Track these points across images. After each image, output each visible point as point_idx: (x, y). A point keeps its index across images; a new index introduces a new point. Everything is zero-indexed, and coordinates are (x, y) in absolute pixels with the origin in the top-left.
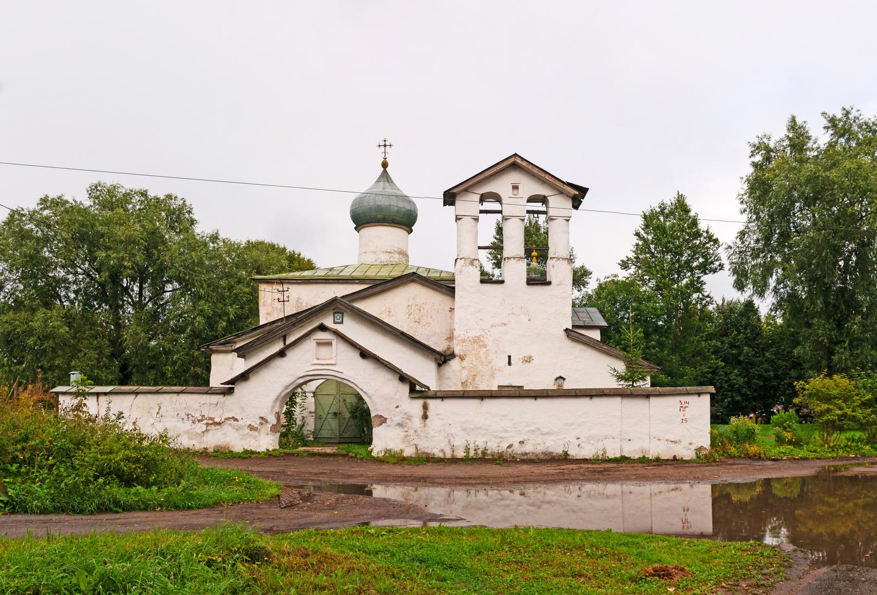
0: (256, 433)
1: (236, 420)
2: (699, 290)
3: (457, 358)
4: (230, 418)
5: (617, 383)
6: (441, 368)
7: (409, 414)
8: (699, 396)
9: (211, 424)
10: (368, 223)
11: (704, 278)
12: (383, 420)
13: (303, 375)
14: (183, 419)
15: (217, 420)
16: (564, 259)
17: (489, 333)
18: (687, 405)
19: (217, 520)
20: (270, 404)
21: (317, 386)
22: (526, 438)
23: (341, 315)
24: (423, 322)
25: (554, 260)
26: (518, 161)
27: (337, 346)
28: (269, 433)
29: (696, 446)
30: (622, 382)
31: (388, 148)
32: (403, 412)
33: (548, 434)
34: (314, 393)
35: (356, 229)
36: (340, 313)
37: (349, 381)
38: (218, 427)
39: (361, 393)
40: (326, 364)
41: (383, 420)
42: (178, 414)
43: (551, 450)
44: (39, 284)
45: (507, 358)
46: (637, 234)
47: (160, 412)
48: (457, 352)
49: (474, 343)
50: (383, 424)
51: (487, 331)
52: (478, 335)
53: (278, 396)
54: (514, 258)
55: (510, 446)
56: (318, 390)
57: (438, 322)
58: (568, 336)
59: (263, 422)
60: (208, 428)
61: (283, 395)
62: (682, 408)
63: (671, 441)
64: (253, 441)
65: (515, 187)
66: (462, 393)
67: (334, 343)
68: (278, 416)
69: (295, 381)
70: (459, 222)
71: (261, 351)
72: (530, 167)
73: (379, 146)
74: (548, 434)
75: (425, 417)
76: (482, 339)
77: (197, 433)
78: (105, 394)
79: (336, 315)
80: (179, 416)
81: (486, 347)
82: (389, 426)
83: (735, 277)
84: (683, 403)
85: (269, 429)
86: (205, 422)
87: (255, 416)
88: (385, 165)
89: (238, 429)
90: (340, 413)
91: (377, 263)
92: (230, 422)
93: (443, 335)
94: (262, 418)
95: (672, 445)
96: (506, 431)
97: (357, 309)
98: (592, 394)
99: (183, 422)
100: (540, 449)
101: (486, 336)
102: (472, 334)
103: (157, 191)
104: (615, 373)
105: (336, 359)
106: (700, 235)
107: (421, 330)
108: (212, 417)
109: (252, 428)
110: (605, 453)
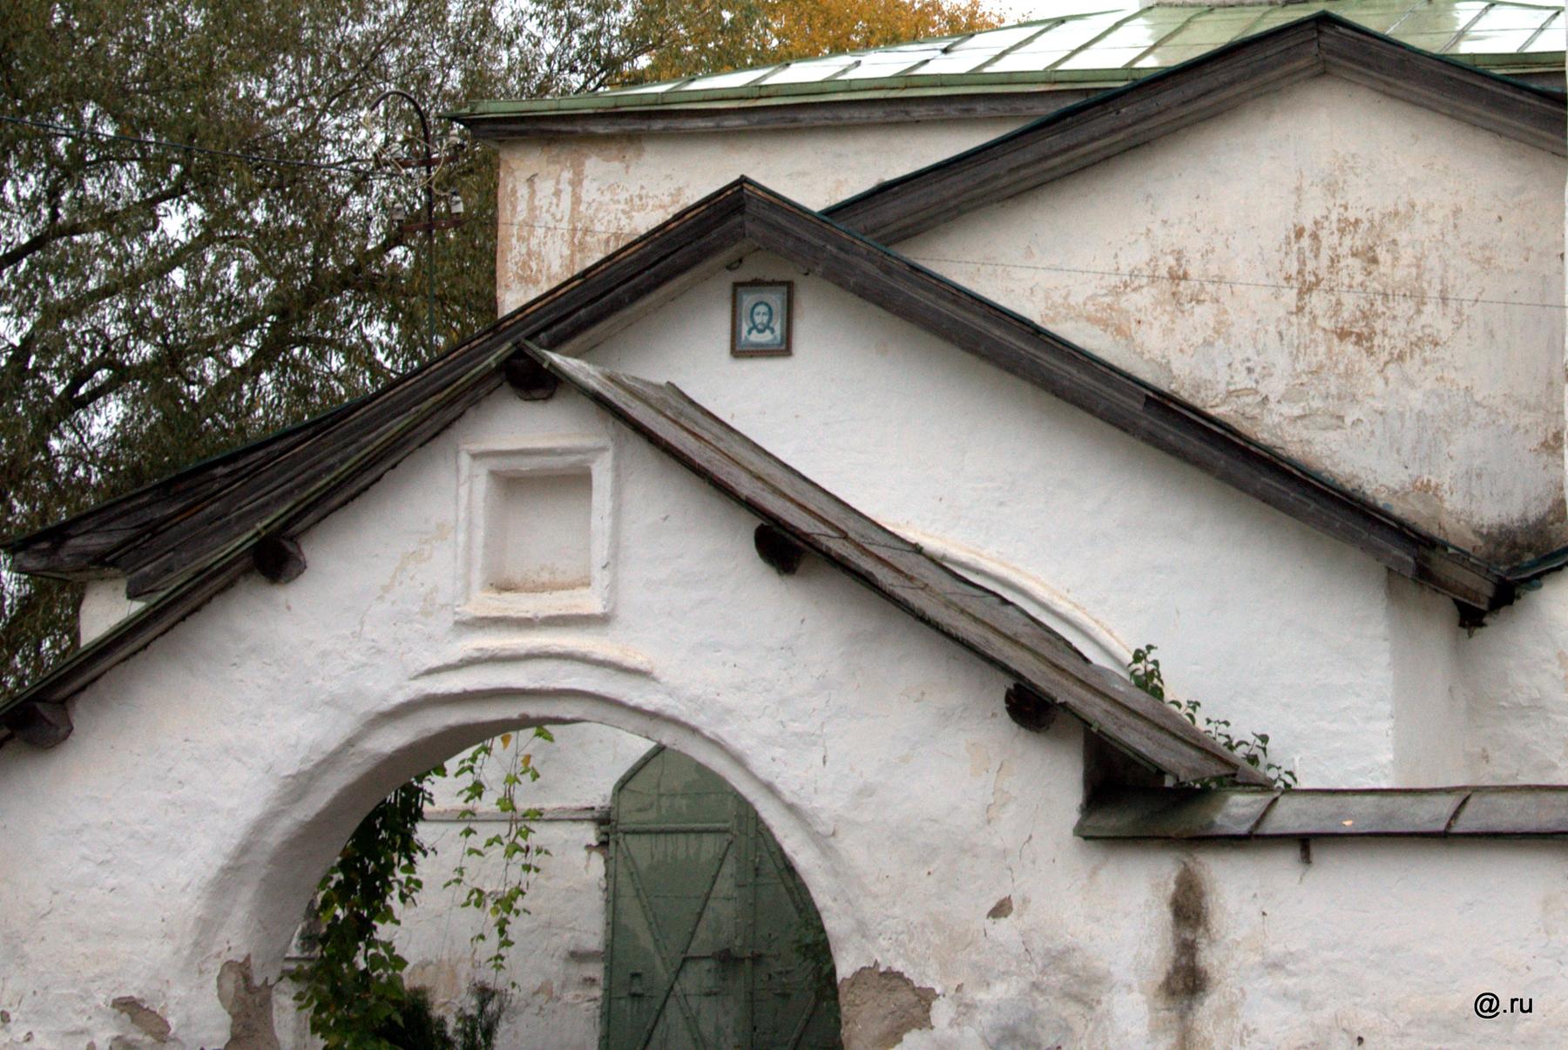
7: (1076, 962)
8: (1306, 858)
13: (399, 698)
20: (190, 905)
24: (1393, 333)
32: (1038, 945)
34: (604, 820)
37: (694, 731)
39: (770, 813)
56: (628, 802)
57: (1491, 334)
61: (275, 838)
66: (1446, 805)
67: (602, 474)
69: (350, 743)
71: (480, 633)
79: (748, 300)
87: (85, 996)
90: (757, 959)
93: (1527, 420)
94: (130, 1007)
97: (1421, 105)
105: (613, 587)
107: (1378, 384)
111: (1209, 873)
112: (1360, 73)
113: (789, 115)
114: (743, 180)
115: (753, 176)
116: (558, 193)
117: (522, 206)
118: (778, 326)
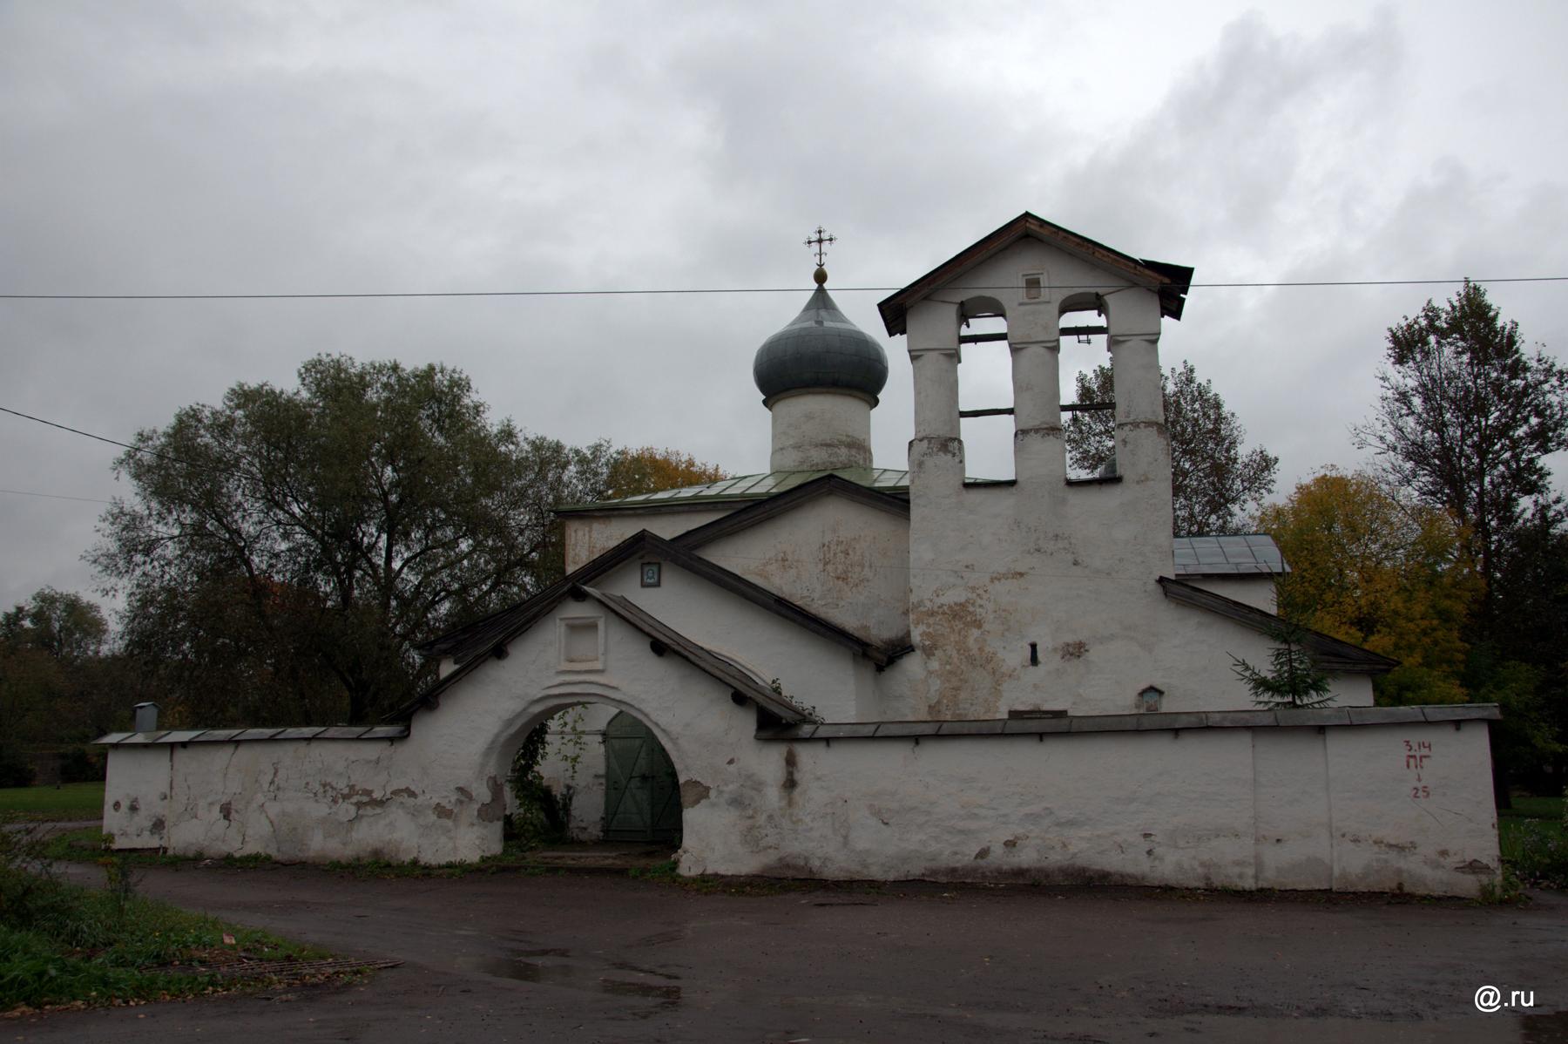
0: (449, 823)
1: (412, 794)
2: (1531, 489)
3: (918, 652)
4: (402, 791)
5: (1254, 698)
6: (884, 674)
9: (365, 804)
10: (788, 389)
11: (1544, 461)
12: (702, 792)
13: (539, 696)
14: (315, 794)
15: (377, 795)
16: (1149, 424)
17: (985, 596)
18: (1424, 752)
21: (609, 718)
22: (1020, 831)
23: (655, 569)
25: (1126, 428)
26: (1032, 227)
27: (606, 632)
28: (475, 821)
29: (1457, 859)
30: (1266, 697)
31: (826, 245)
33: (1072, 823)
35: (765, 402)
36: (655, 563)
38: (378, 810)
41: (702, 792)
42: (307, 784)
43: (1081, 862)
45: (1029, 648)
47: (276, 779)
48: (916, 637)
49: (954, 617)
50: (703, 802)
51: (980, 592)
52: (963, 600)
53: (493, 742)
54: (1037, 431)
55: (983, 854)
58: (1166, 594)
59: (463, 798)
60: (360, 812)
61: (502, 739)
62: (1412, 761)
63: (1390, 846)
64: (443, 839)
65: (1033, 284)
66: (873, 728)
68: (496, 789)
69: (525, 709)
70: (920, 363)
72: (524, 629)
73: (809, 242)
74: (1072, 823)
75: (790, 784)
76: (971, 609)
77: (341, 823)
78: (184, 745)
79: (646, 569)
80: (310, 787)
81: (980, 627)
82: (713, 805)
84: (1415, 747)
85: (476, 813)
86: (355, 799)
88: (821, 277)
89: (415, 813)
91: (805, 467)
92: (401, 799)
94: (460, 790)
95: (1392, 856)
96: (975, 816)
98: (1177, 726)
99: (317, 801)
100: (1056, 859)
101: (979, 602)
102: (952, 597)
103: (412, 363)
104: (1247, 674)
106: (1526, 369)
108: (369, 788)
109: (442, 812)
113: (657, 509)
115: (647, 529)
116: (584, 535)
117: (573, 539)
118: (656, 577)
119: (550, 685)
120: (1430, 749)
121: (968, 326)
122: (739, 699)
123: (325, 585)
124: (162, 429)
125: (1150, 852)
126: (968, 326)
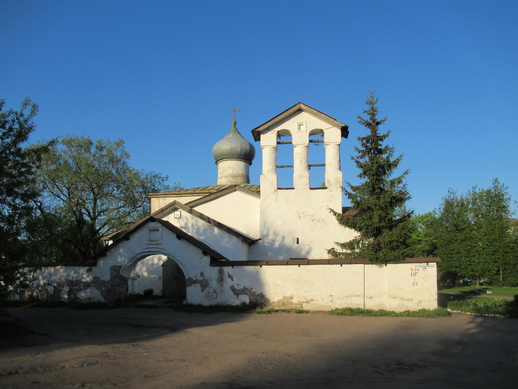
18: (417, 271)
19: (374, 142)
37: (170, 255)
40: (155, 244)
44: (8, 256)
46: (154, 171)
69: (135, 256)
83: (142, 294)
110: (308, 253)
111: (303, 254)
112: (203, 241)
114: (175, 201)
115: (176, 200)
117: (154, 204)
119: (144, 248)
120: (418, 271)
121: (280, 139)
122: (205, 253)
123: (38, 208)
124: (304, 308)
125: (331, 301)
126: (280, 139)
